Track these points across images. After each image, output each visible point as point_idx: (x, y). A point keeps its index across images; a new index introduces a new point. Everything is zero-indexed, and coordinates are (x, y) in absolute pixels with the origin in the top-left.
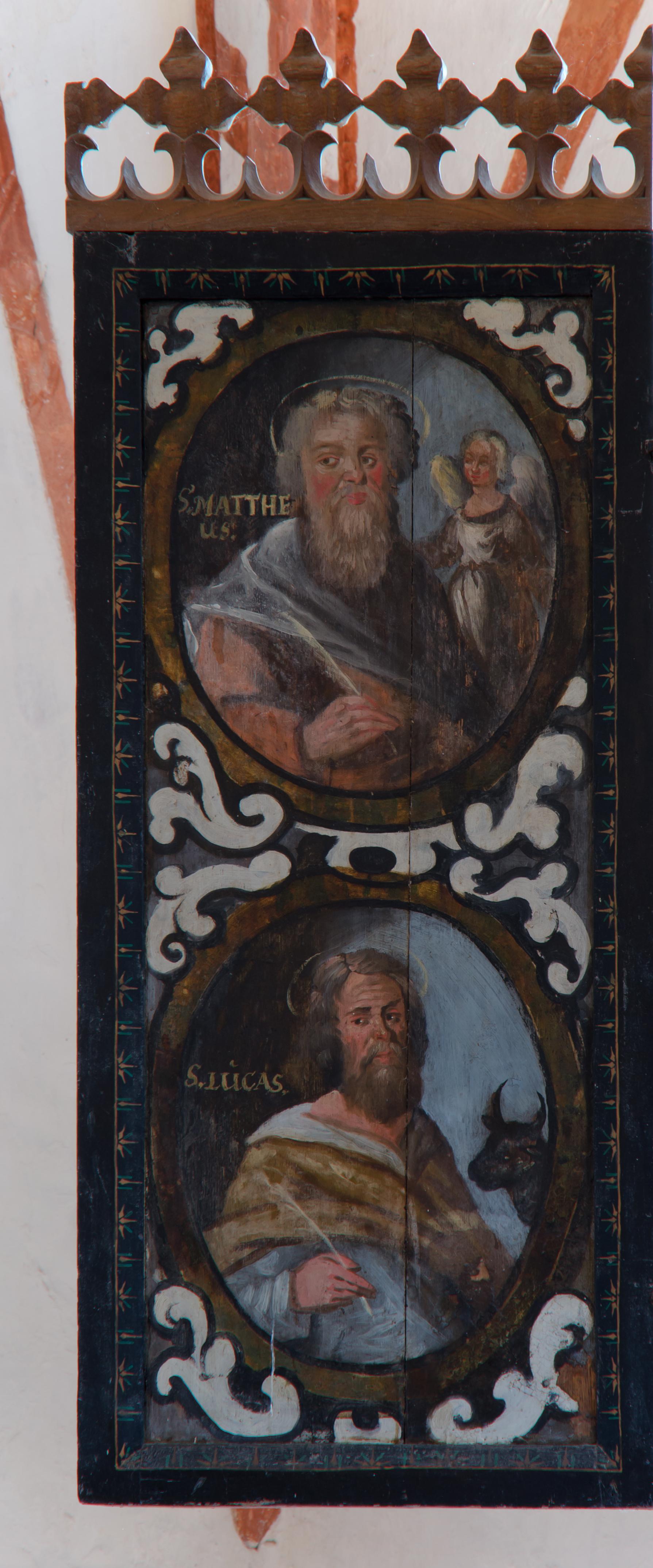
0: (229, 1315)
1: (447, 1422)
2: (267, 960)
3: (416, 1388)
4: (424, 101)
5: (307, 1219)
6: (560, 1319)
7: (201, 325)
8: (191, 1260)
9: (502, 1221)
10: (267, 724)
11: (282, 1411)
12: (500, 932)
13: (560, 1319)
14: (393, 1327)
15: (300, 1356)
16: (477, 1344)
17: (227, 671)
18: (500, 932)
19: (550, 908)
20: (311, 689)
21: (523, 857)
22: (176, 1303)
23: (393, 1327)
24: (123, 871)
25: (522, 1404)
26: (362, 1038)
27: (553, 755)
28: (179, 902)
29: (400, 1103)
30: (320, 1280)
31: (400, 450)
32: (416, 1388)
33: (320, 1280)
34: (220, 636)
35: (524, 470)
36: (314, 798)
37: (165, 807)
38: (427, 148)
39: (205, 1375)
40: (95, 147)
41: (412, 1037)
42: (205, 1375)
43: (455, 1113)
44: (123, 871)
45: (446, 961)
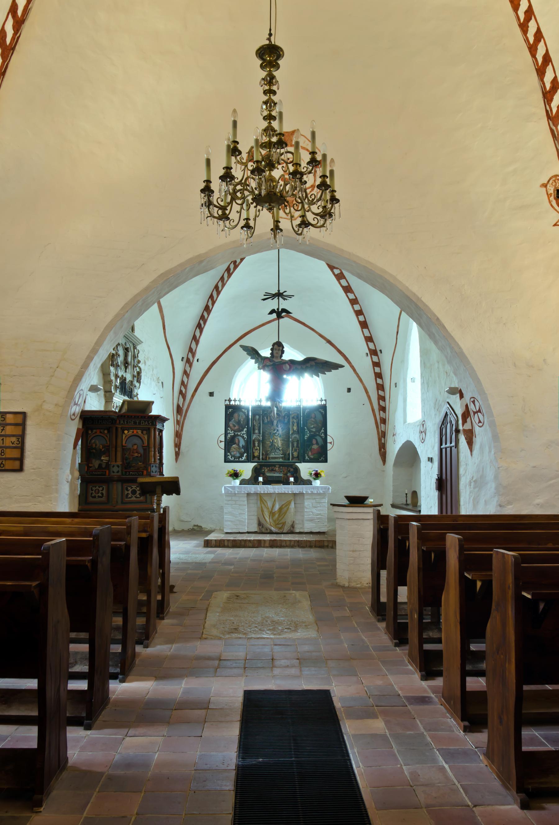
0: (231, 454)
1: (240, 459)
2: (233, 438)
3: (239, 458)
4: (235, 400)
5: (234, 450)
6: (245, 454)
7: (230, 410)
8: (229, 452)
9: (243, 450)
10: (233, 428)
11: (233, 459)
12: (243, 437)
13: (245, 454)
14: (238, 455)
15: (234, 456)
16: (242, 456)
17: (231, 425)
18: (243, 437)
19: (245, 436)
20: (235, 426)
21: (244, 434)
22: (229, 454)
23: (238, 455)
24: (257, 417)
25: (244, 458)
26: (237, 442)
27: (245, 429)
28: (229, 436)
29: (238, 445)
30: (235, 453)
31: (239, 416)
32: (239, 458)
33: (235, 453)
34: (231, 424)
35: (244, 417)
36: (235, 431)
37: (228, 431)
38: (230, 402)
39: (230, 457)
40: (153, 402)
41: (239, 441)
42: (230, 457)
43: (241, 445)
44: (257, 417)
45: (241, 438)
